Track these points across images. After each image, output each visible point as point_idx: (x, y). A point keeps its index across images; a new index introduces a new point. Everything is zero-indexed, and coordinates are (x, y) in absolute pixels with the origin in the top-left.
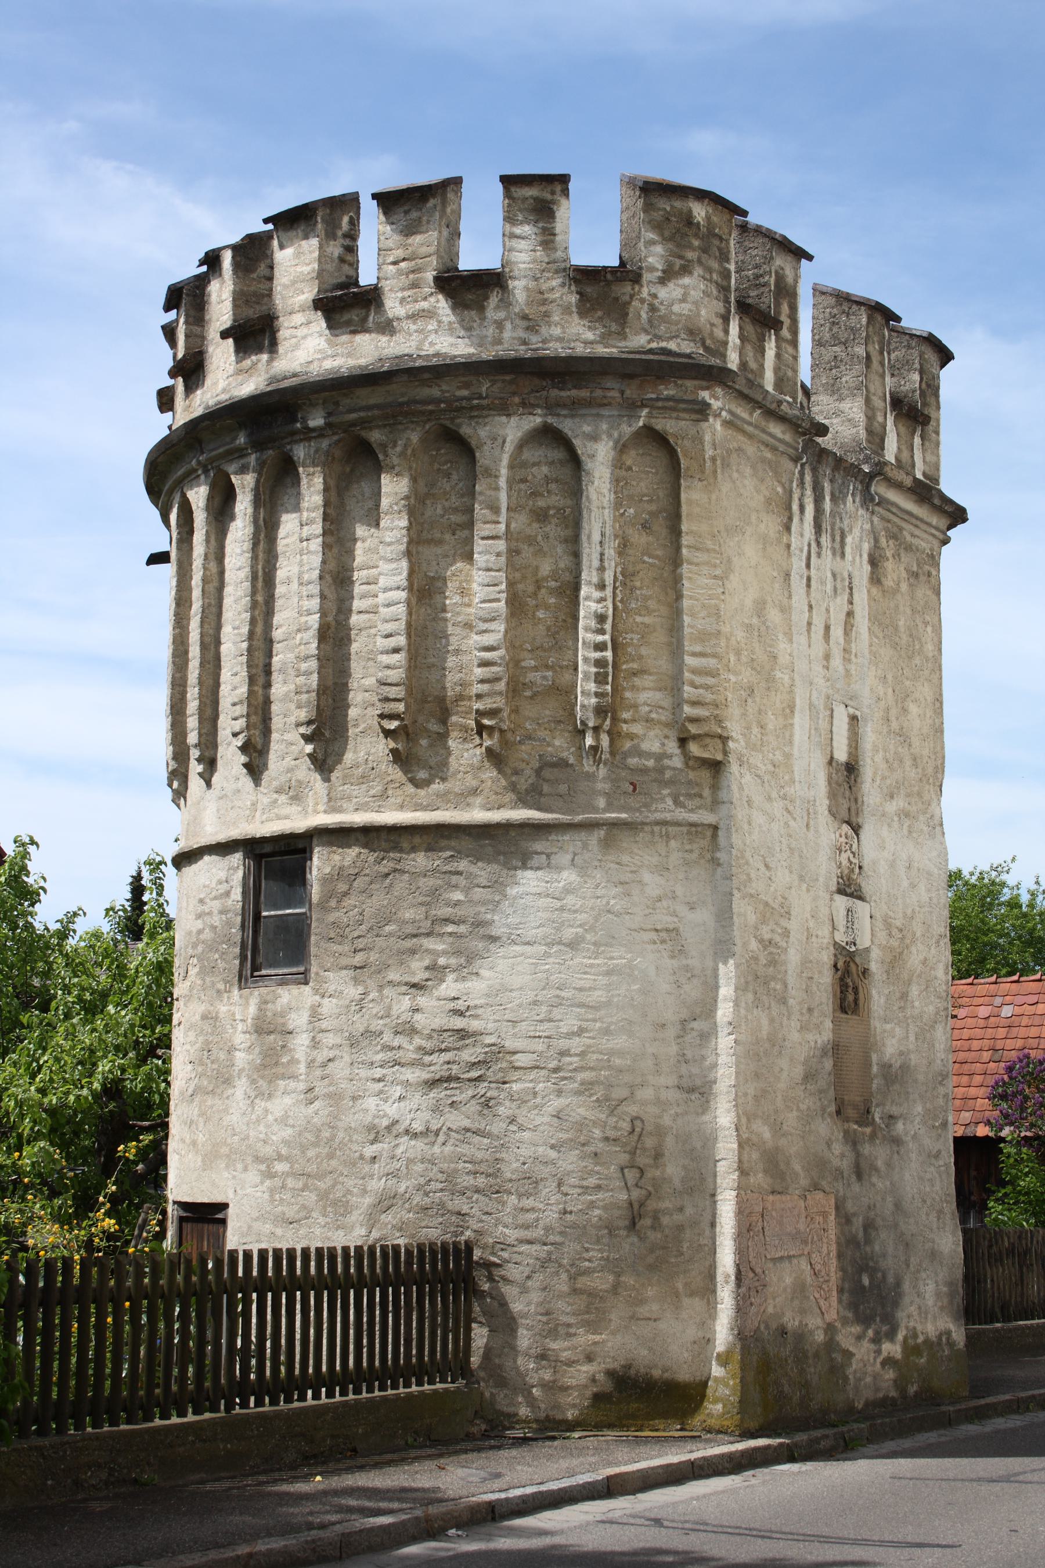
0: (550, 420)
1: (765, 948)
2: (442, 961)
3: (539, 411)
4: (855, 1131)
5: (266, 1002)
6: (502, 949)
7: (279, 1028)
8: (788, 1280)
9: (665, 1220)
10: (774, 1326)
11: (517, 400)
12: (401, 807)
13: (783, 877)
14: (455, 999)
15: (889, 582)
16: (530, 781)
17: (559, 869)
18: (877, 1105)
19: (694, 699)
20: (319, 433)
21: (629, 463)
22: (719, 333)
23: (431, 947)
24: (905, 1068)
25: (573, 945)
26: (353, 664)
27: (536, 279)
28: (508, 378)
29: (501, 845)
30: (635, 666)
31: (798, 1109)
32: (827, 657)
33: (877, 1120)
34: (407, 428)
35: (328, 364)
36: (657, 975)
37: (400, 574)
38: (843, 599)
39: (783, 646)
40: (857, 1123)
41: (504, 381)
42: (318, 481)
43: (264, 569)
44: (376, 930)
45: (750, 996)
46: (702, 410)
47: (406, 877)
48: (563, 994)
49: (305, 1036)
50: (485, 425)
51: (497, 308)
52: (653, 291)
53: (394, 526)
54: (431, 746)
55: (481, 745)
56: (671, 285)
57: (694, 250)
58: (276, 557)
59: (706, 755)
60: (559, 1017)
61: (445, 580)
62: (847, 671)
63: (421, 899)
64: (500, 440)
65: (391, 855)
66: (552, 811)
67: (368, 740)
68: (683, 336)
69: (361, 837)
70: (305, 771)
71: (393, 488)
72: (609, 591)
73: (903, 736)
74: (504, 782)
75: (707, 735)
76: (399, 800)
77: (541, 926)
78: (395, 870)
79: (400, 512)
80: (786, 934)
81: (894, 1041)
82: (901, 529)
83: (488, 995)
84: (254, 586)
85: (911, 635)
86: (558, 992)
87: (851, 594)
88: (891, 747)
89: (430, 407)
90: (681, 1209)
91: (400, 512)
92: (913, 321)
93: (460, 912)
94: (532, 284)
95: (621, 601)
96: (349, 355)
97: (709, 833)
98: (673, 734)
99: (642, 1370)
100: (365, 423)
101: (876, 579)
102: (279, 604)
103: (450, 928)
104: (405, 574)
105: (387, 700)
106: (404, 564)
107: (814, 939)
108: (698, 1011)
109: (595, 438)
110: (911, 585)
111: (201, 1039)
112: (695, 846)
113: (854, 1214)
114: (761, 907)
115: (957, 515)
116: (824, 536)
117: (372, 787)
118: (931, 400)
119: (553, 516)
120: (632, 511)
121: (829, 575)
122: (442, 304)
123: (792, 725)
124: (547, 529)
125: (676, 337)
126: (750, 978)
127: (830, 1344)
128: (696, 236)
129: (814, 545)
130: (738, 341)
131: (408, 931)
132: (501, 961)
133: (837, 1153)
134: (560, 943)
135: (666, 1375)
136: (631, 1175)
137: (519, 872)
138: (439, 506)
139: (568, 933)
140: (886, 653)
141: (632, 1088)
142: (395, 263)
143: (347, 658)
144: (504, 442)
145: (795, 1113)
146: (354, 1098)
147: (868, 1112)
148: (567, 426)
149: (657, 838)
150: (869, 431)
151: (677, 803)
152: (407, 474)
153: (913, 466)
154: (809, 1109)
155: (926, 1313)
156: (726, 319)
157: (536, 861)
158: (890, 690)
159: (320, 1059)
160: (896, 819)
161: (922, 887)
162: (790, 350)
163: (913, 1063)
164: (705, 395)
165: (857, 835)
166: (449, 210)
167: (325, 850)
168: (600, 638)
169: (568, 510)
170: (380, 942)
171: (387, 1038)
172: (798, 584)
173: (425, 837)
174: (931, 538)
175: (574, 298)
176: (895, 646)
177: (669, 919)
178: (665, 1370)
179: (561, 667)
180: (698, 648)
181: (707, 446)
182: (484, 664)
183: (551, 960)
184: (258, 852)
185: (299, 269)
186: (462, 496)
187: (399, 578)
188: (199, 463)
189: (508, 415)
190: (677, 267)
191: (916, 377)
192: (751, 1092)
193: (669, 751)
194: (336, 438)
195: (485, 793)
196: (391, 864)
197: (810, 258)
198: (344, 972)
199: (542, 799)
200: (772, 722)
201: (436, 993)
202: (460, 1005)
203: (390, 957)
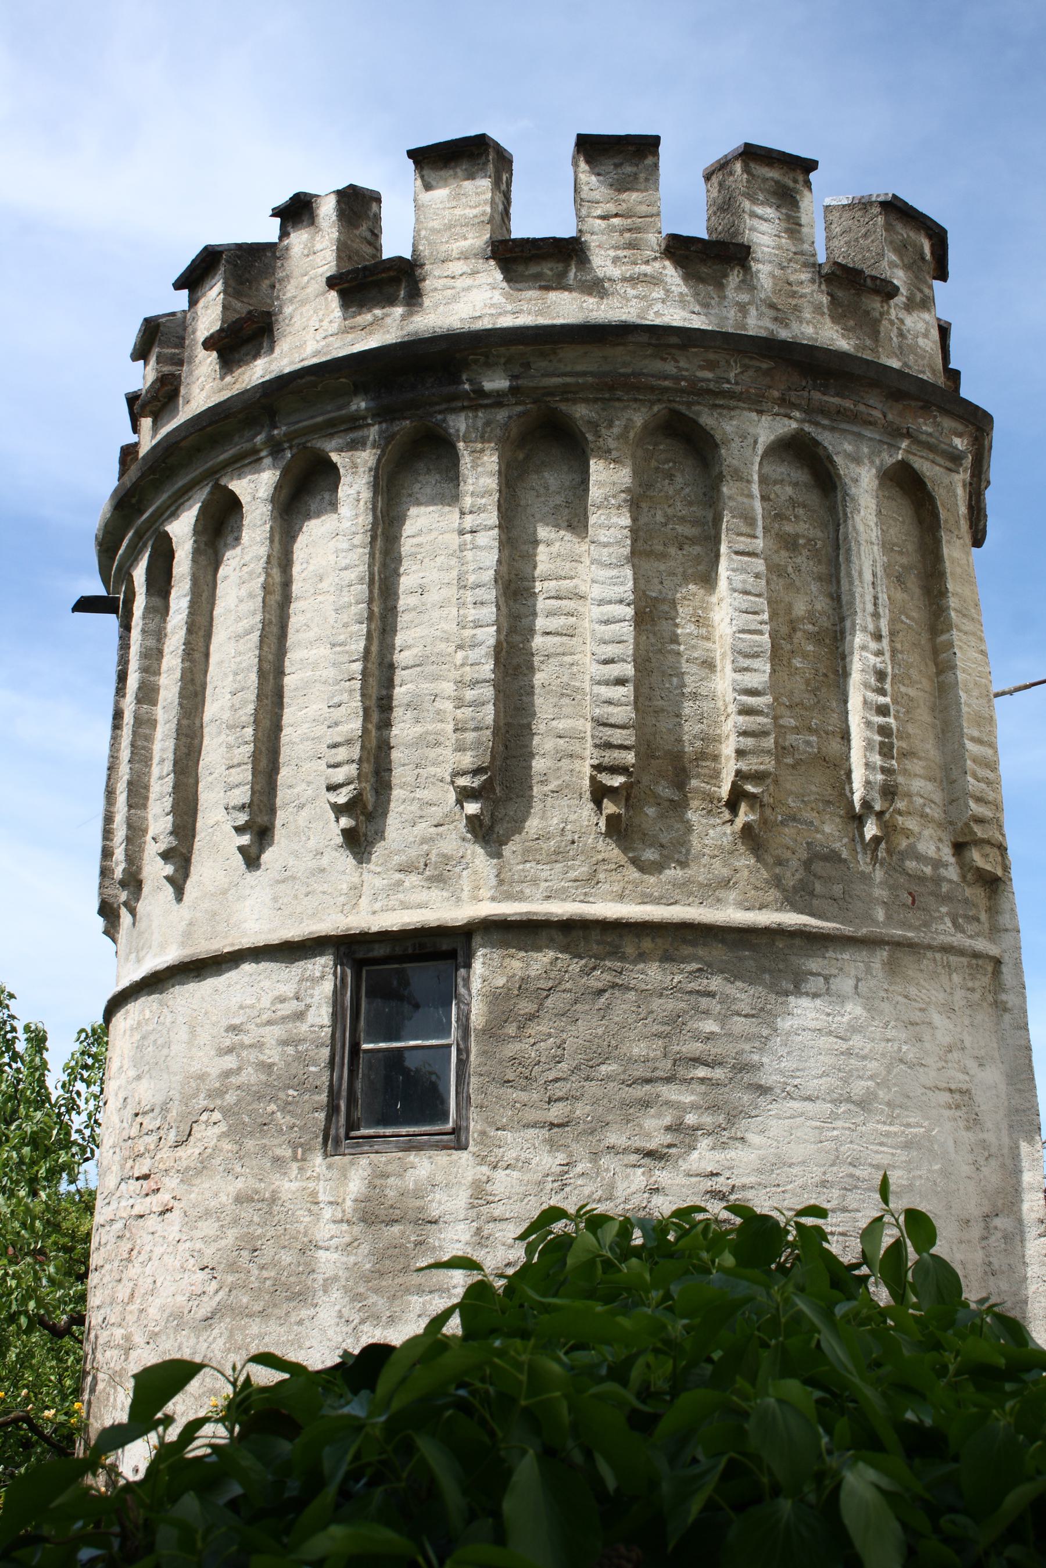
0: (807, 427)
2: (690, 1119)
3: (797, 414)
5: (385, 1176)
6: (774, 1106)
7: (411, 1215)
12: (621, 897)
14: (713, 1174)
16: (798, 876)
17: (842, 999)
19: (978, 794)
20: (498, 400)
23: (673, 1097)
25: (864, 1104)
26: (538, 701)
27: (783, 268)
28: (764, 366)
29: (766, 958)
34: (626, 408)
37: (622, 584)
41: (758, 369)
42: (491, 461)
43: (380, 573)
44: (586, 1069)
47: (631, 995)
48: (858, 1172)
49: (461, 1226)
50: (731, 418)
51: (738, 289)
52: (900, 316)
53: (610, 524)
54: (662, 816)
55: (732, 821)
58: (399, 560)
60: (854, 1206)
61: (673, 603)
63: (656, 1028)
64: (751, 440)
65: (608, 963)
66: (827, 920)
67: (565, 802)
69: (559, 937)
70: (454, 840)
71: (606, 478)
72: (885, 642)
74: (765, 875)
77: (825, 1074)
78: (614, 986)
79: (619, 507)
83: (759, 1171)
86: (851, 1169)
89: (667, 383)
91: (619, 507)
93: (715, 1049)
94: (778, 272)
96: (539, 313)
98: (947, 838)
100: (568, 393)
102: (403, 620)
103: (701, 1072)
104: (630, 584)
105: (608, 746)
106: (628, 572)
109: (857, 460)
111: (232, 1233)
112: (977, 984)
119: (804, 546)
122: (670, 273)
124: (799, 560)
132: (774, 1122)
134: (849, 1100)
137: (791, 999)
138: (659, 512)
139: (859, 1087)
142: (604, 218)
143: (530, 691)
144: (756, 442)
148: (827, 439)
149: (940, 969)
152: (629, 462)
157: (815, 984)
167: (497, 954)
168: (882, 700)
169: (819, 543)
170: (592, 1088)
173: (659, 941)
175: (825, 299)
177: (962, 1077)
179: (827, 733)
180: (976, 733)
183: (839, 1124)
184: (360, 955)
185: (458, 212)
186: (690, 504)
187: (622, 589)
188: (270, 439)
189: (760, 412)
194: (520, 408)
196: (607, 977)
198: (532, 1132)
199: (815, 902)
201: (684, 1166)
203: (609, 1110)
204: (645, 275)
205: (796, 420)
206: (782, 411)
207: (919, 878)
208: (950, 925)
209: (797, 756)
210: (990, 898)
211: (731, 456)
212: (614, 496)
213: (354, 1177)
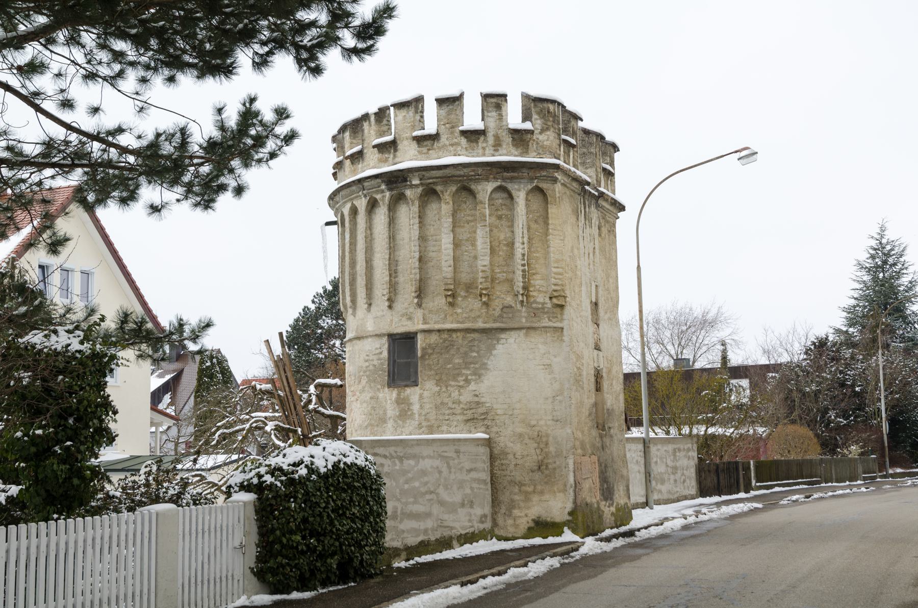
9: (550, 466)
12: (452, 323)
20: (416, 186)
24: (613, 410)
46: (555, 180)
73: (608, 290)
80: (583, 365)
92: (608, 138)
101: (600, 235)
109: (519, 190)
127: (599, 508)
136: (538, 451)
140: (603, 261)
146: (438, 427)
148: (509, 186)
151: (549, 320)
157: (502, 341)
159: (424, 413)
164: (556, 174)
171: (450, 405)
172: (581, 239)
176: (605, 258)
180: (556, 265)
182: (483, 271)
211: (480, 196)
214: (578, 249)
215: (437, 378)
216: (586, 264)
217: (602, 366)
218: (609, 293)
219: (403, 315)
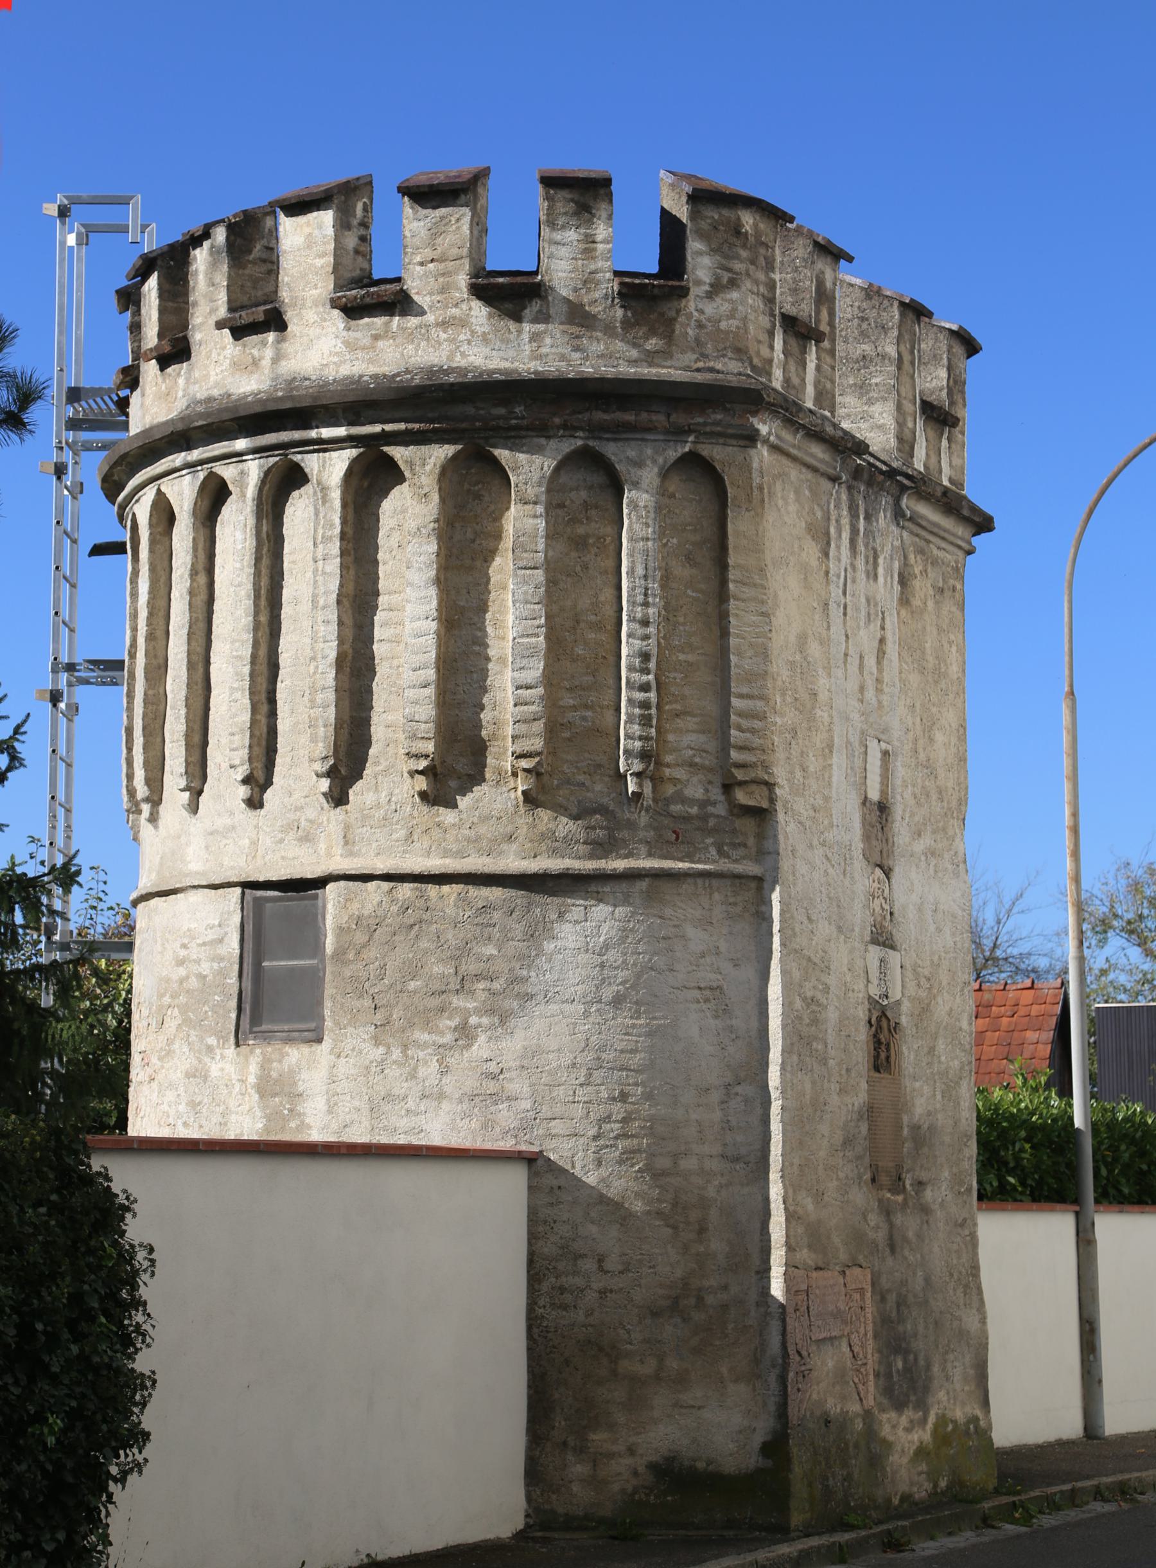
0: (591, 443)
1: (808, 1006)
2: (473, 1020)
4: (888, 1199)
8: (831, 1364)
9: (710, 1300)
10: (818, 1413)
11: (557, 420)
13: (824, 929)
15: (916, 602)
18: (908, 1171)
19: (740, 744)
21: (671, 489)
22: (765, 352)
24: (932, 1128)
30: (678, 707)
31: (838, 1179)
32: (862, 689)
33: (908, 1186)
35: (345, 371)
36: (701, 1036)
38: (875, 626)
39: (823, 682)
40: (889, 1190)
45: (795, 1058)
46: (751, 438)
52: (700, 306)
56: (718, 300)
57: (742, 262)
59: (752, 803)
62: (880, 702)
68: (730, 354)
75: (753, 782)
76: (426, 845)
81: (923, 1100)
82: (928, 542)
84: (256, 605)
85: (937, 658)
87: (883, 619)
88: (919, 781)
89: (464, 425)
90: (725, 1288)
95: (664, 638)
97: (753, 885)
98: (718, 780)
99: (686, 1463)
101: (904, 601)
107: (850, 994)
108: (742, 1074)
109: (639, 464)
110: (937, 603)
112: (739, 898)
113: (889, 1291)
114: (804, 963)
115: (983, 524)
116: (858, 558)
117: (396, 831)
118: (957, 397)
120: (675, 541)
121: (863, 600)
122: (479, 311)
123: (830, 765)
125: (724, 356)
126: (795, 1039)
127: (871, 1432)
128: (744, 246)
129: (849, 569)
130: (782, 356)
131: (435, 988)
133: (872, 1224)
135: (711, 1468)
140: (914, 679)
141: (675, 1157)
142: (422, 264)
145: (835, 1183)
147: (900, 1179)
148: (611, 450)
150: (900, 439)
151: (721, 853)
153: (940, 472)
154: (847, 1177)
155: (955, 1398)
156: (771, 334)
158: (918, 719)
160: (923, 858)
161: (947, 931)
162: (828, 360)
163: (940, 1123)
165: (888, 879)
166: (479, 206)
168: (645, 678)
172: (836, 613)
174: (956, 550)
176: (922, 671)
177: (713, 976)
178: (709, 1462)
179: (602, 707)
181: (755, 475)
189: (548, 437)
190: (725, 281)
191: (943, 374)
192: (796, 1161)
193: (713, 798)
195: (521, 839)
197: (850, 259)
200: (813, 765)
202: (493, 1067)
204: (454, 318)
205: (581, 438)
206: (567, 433)
207: (684, 818)
208: (714, 853)
209: (573, 730)
210: (759, 826)
212: (425, 527)
213: (255, 1056)
214: (825, 642)
215: (379, 1018)
216: (852, 685)
217: (896, 994)
218: (933, 774)
219: (285, 829)
